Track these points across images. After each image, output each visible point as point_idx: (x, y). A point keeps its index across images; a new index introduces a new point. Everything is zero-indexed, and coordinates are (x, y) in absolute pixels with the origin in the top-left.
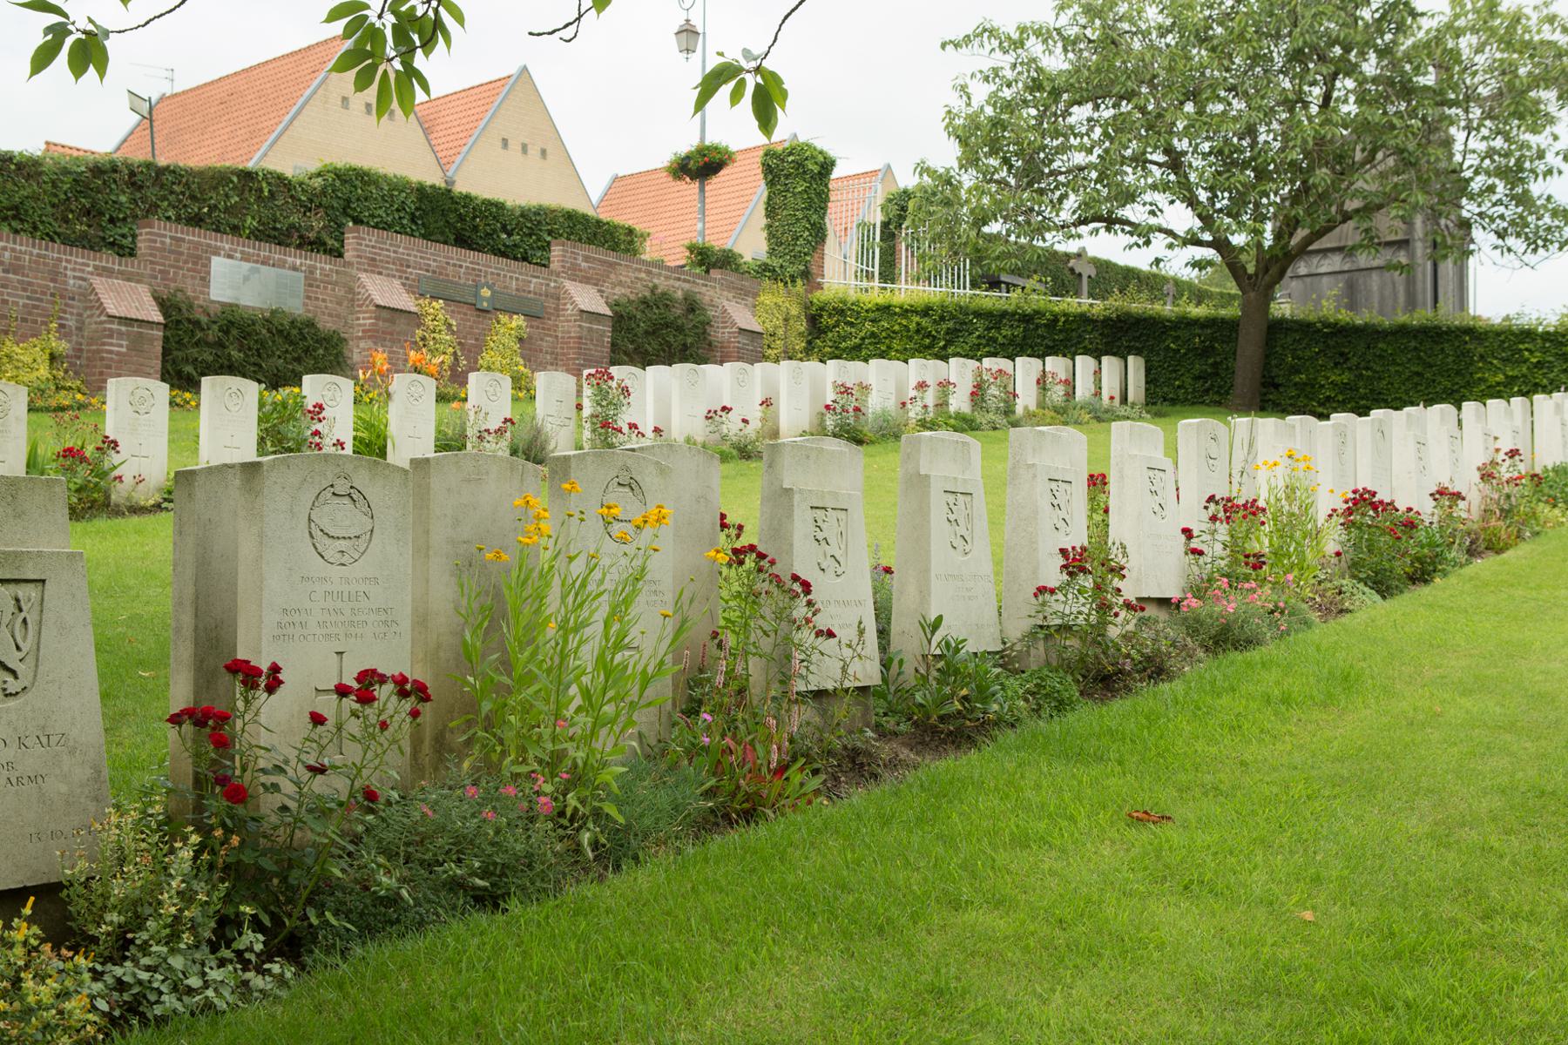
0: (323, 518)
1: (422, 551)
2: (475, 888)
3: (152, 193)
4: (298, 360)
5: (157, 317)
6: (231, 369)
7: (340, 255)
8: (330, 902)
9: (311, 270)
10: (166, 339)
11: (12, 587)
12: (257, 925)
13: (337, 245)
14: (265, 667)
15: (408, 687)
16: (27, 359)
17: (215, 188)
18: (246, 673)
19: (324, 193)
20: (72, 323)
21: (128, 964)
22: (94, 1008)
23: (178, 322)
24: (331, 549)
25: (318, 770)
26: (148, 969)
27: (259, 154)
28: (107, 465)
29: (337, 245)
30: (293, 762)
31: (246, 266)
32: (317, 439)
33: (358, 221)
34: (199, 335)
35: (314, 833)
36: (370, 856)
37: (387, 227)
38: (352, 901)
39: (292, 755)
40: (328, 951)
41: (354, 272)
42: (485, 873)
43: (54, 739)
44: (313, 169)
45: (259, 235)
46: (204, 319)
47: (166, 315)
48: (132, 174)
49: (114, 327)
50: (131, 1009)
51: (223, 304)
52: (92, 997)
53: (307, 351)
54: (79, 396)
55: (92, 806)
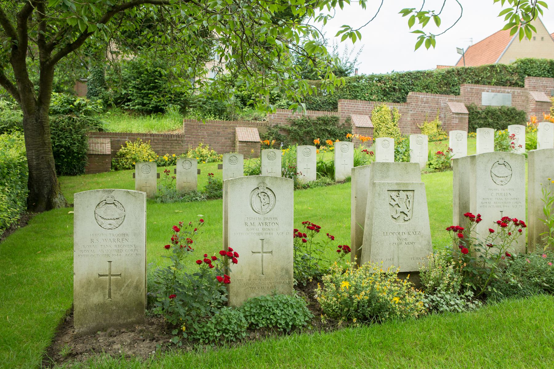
0: (495, 171)
1: (532, 179)
2: (544, 286)
3: (464, 76)
4: (510, 120)
5: (466, 112)
6: (488, 125)
7: (523, 87)
8: (496, 285)
9: (514, 93)
10: (469, 118)
11: (406, 192)
12: (472, 288)
13: (522, 84)
14: (476, 216)
15: (518, 222)
16: (431, 127)
17: (483, 72)
18: (469, 216)
19: (517, 68)
20: (442, 116)
21: (435, 295)
22: (424, 306)
23: (473, 113)
24: (498, 180)
25: (491, 246)
26: (440, 297)
27: (498, 60)
28: (449, 156)
29: (522, 84)
30: (484, 243)
31: (493, 94)
32: (513, 145)
33: (529, 75)
34: (479, 116)
35: (490, 265)
36: (509, 274)
37: (539, 76)
38: (503, 286)
39: (484, 241)
40: (493, 299)
41: (528, 91)
42: (548, 282)
43: (417, 233)
44: (514, 61)
45: (497, 84)
46: (480, 111)
47: (469, 111)
48: (458, 71)
49: (454, 116)
50: (435, 308)
51: (486, 106)
52: (424, 303)
53: (513, 117)
54: (445, 136)
55: (427, 252)
